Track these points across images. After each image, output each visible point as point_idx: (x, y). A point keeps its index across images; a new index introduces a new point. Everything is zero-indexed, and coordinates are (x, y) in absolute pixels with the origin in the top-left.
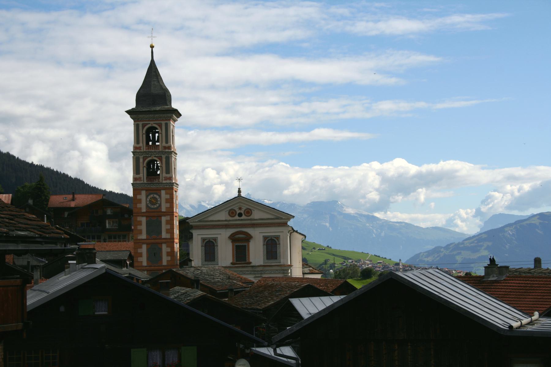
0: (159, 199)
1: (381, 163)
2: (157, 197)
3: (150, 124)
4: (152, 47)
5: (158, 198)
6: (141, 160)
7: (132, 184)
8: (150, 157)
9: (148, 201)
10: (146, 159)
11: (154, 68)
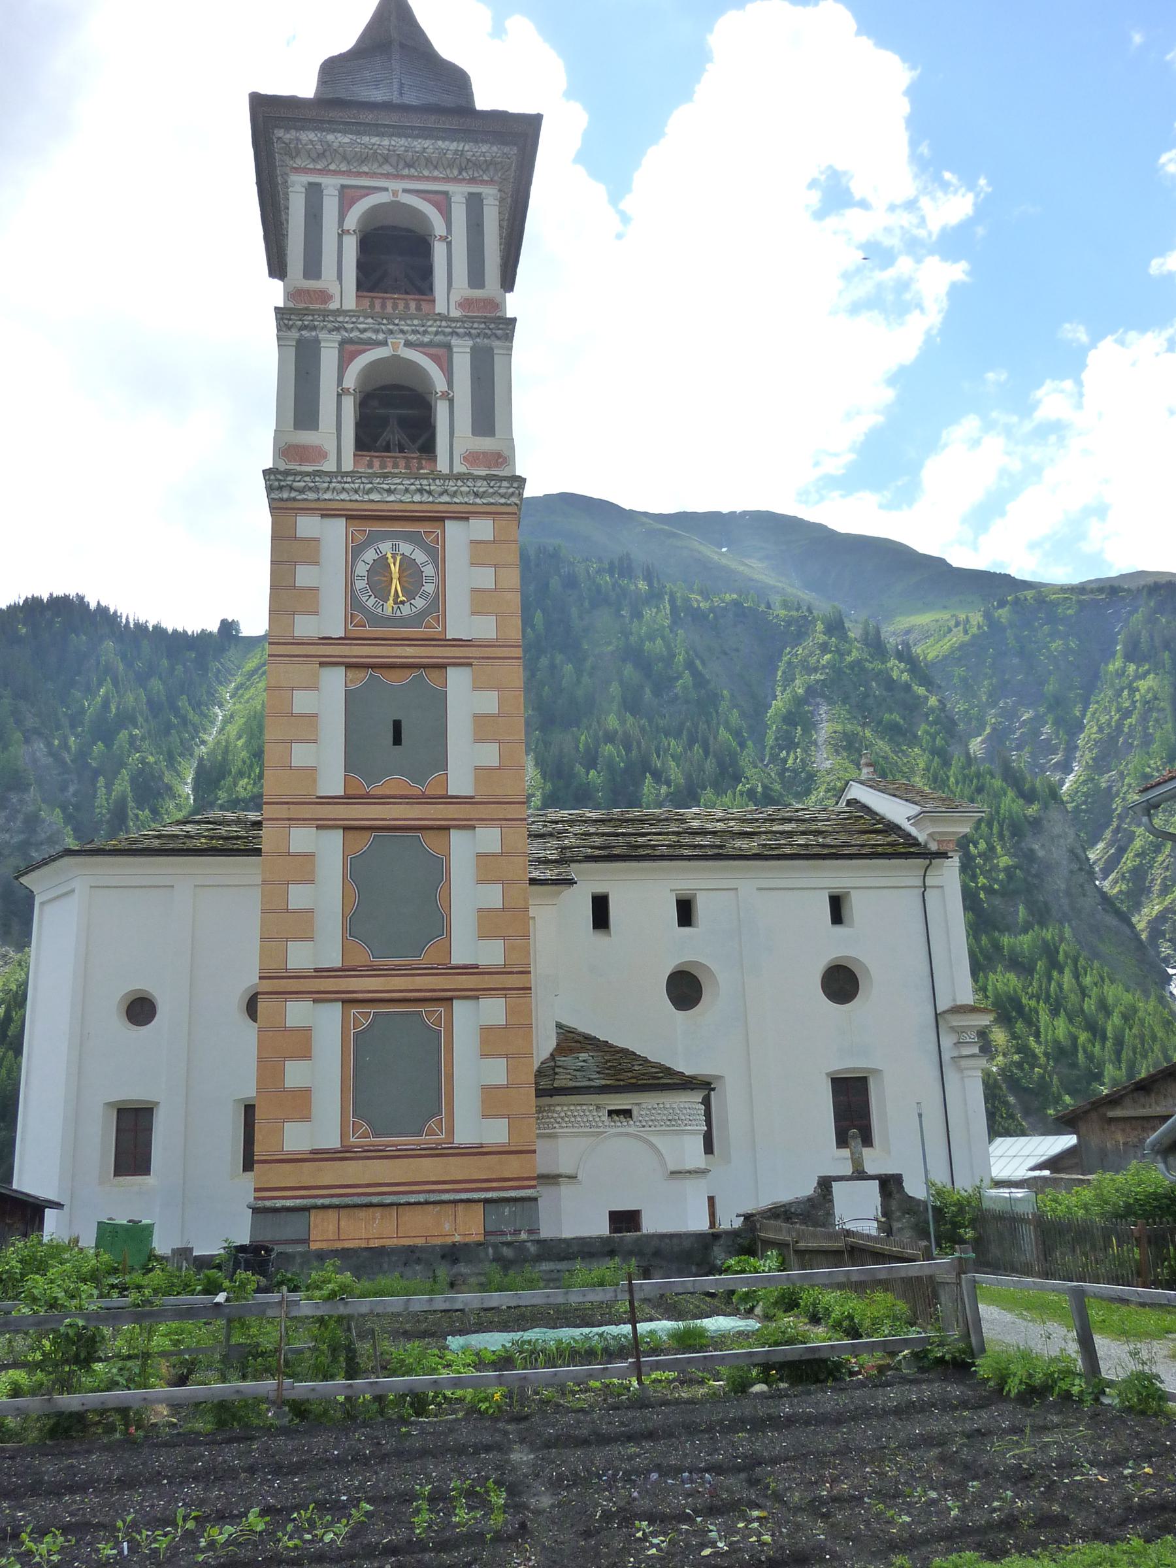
0: (429, 571)
1: (569, 94)
3: (386, 189)
5: (425, 564)
6: (329, 357)
7: (277, 310)
8: (384, 343)
9: (361, 578)
10: (353, 356)
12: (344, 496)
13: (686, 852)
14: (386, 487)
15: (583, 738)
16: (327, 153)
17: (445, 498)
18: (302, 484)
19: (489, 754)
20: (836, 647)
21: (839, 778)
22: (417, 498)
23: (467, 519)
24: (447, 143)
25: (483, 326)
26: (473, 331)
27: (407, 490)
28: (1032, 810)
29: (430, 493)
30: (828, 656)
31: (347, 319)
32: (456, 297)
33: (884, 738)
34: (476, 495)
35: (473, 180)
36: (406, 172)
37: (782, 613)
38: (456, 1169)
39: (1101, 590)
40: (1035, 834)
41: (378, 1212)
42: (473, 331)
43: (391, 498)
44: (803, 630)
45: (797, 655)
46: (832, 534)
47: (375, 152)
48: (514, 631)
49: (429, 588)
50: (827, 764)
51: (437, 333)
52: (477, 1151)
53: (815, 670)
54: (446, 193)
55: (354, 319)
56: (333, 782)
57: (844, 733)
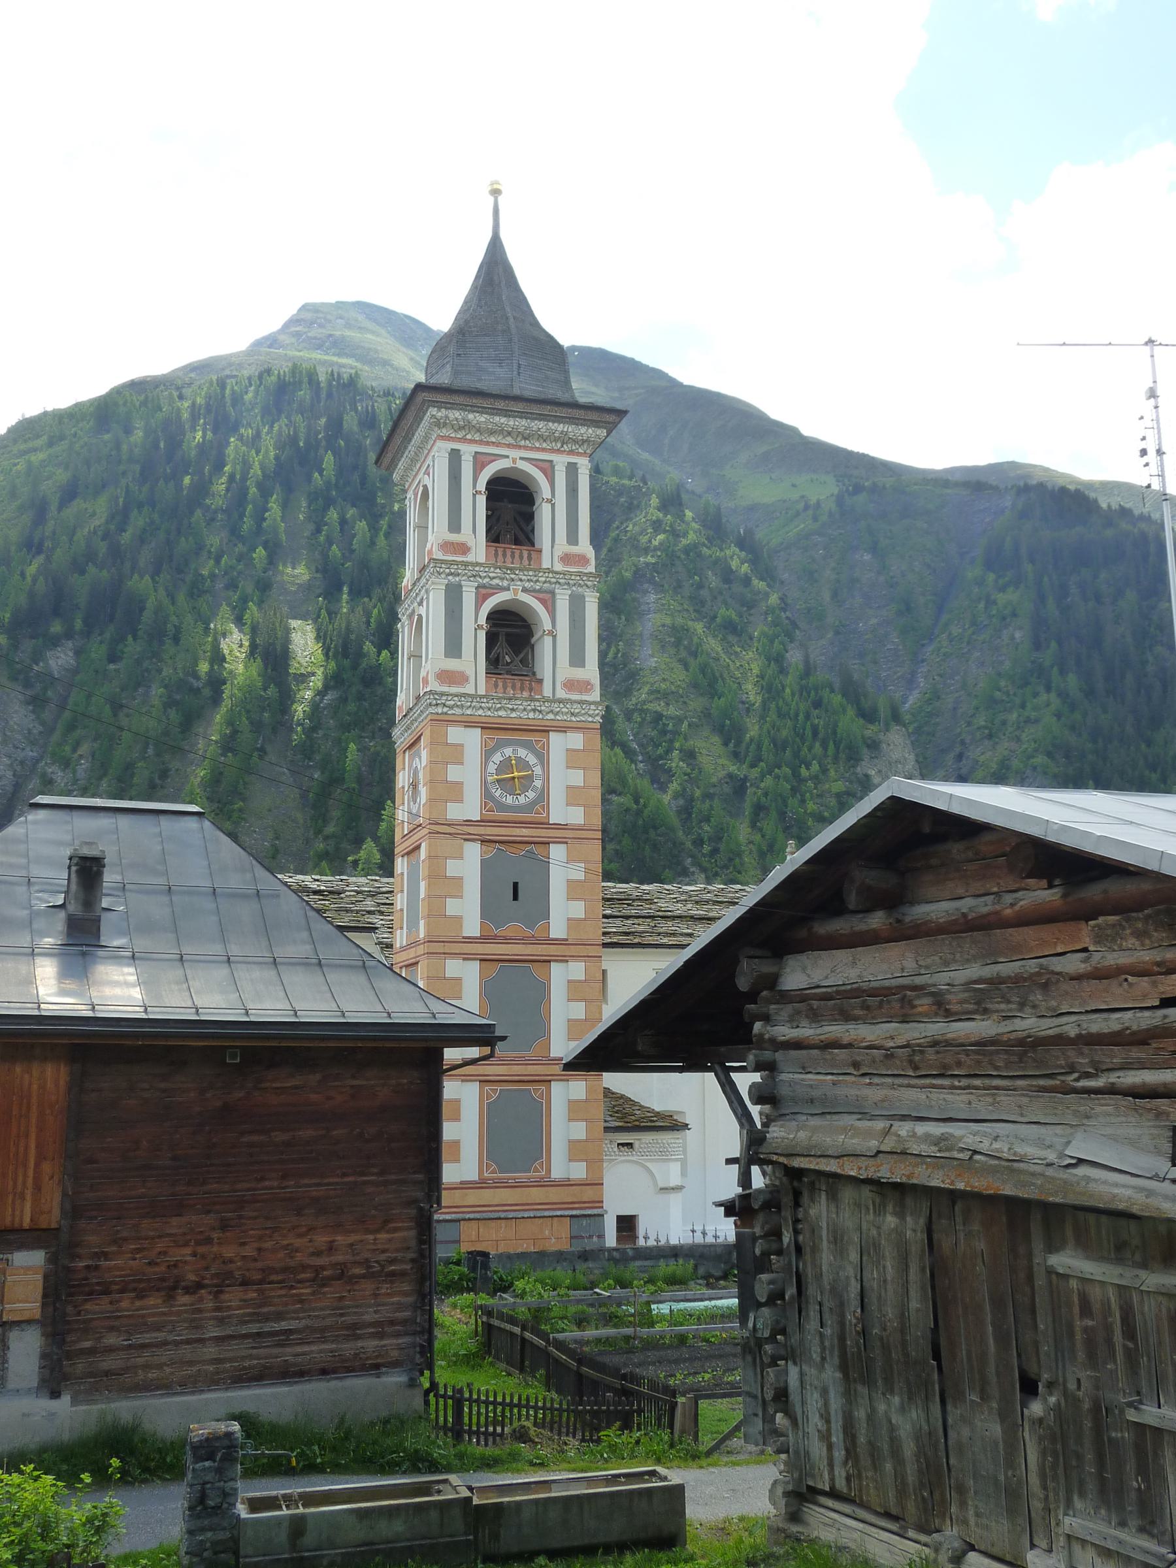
0: (538, 770)
2: (532, 759)
3: (507, 457)
4: (496, 192)
11: (168, 1370)
12: (480, 712)
13: (665, 940)
14: (511, 707)
15: (375, 611)
16: (467, 427)
17: (551, 716)
18: (453, 703)
19: (578, 909)
20: (671, 526)
21: (664, 680)
22: (531, 715)
23: (565, 732)
24: (556, 424)
25: (578, 578)
26: (571, 582)
27: (525, 709)
28: (871, 731)
29: (540, 712)
30: (661, 537)
31: (482, 569)
32: (558, 553)
33: (717, 636)
34: (572, 714)
35: (571, 452)
36: (522, 443)
37: (613, 480)
38: (554, 1195)
39: (966, 484)
40: (872, 758)
41: (503, 1223)
42: (571, 582)
43: (514, 715)
44: (635, 502)
45: (626, 532)
46: (673, 383)
47: (503, 429)
48: (597, 821)
49: (538, 783)
50: (652, 662)
51: (545, 582)
52: (566, 1183)
53: (646, 551)
54: (551, 461)
55: (487, 569)
56: (472, 927)
57: (673, 627)
